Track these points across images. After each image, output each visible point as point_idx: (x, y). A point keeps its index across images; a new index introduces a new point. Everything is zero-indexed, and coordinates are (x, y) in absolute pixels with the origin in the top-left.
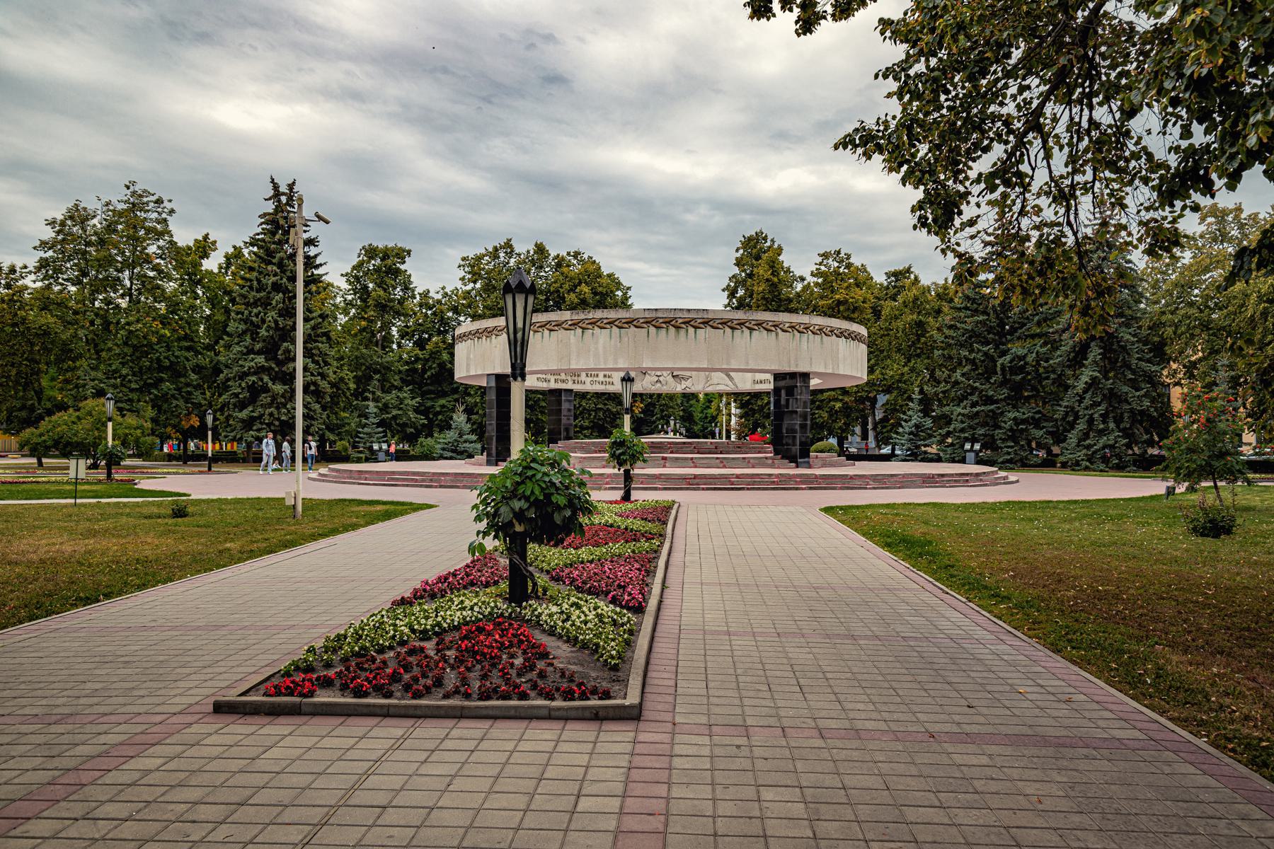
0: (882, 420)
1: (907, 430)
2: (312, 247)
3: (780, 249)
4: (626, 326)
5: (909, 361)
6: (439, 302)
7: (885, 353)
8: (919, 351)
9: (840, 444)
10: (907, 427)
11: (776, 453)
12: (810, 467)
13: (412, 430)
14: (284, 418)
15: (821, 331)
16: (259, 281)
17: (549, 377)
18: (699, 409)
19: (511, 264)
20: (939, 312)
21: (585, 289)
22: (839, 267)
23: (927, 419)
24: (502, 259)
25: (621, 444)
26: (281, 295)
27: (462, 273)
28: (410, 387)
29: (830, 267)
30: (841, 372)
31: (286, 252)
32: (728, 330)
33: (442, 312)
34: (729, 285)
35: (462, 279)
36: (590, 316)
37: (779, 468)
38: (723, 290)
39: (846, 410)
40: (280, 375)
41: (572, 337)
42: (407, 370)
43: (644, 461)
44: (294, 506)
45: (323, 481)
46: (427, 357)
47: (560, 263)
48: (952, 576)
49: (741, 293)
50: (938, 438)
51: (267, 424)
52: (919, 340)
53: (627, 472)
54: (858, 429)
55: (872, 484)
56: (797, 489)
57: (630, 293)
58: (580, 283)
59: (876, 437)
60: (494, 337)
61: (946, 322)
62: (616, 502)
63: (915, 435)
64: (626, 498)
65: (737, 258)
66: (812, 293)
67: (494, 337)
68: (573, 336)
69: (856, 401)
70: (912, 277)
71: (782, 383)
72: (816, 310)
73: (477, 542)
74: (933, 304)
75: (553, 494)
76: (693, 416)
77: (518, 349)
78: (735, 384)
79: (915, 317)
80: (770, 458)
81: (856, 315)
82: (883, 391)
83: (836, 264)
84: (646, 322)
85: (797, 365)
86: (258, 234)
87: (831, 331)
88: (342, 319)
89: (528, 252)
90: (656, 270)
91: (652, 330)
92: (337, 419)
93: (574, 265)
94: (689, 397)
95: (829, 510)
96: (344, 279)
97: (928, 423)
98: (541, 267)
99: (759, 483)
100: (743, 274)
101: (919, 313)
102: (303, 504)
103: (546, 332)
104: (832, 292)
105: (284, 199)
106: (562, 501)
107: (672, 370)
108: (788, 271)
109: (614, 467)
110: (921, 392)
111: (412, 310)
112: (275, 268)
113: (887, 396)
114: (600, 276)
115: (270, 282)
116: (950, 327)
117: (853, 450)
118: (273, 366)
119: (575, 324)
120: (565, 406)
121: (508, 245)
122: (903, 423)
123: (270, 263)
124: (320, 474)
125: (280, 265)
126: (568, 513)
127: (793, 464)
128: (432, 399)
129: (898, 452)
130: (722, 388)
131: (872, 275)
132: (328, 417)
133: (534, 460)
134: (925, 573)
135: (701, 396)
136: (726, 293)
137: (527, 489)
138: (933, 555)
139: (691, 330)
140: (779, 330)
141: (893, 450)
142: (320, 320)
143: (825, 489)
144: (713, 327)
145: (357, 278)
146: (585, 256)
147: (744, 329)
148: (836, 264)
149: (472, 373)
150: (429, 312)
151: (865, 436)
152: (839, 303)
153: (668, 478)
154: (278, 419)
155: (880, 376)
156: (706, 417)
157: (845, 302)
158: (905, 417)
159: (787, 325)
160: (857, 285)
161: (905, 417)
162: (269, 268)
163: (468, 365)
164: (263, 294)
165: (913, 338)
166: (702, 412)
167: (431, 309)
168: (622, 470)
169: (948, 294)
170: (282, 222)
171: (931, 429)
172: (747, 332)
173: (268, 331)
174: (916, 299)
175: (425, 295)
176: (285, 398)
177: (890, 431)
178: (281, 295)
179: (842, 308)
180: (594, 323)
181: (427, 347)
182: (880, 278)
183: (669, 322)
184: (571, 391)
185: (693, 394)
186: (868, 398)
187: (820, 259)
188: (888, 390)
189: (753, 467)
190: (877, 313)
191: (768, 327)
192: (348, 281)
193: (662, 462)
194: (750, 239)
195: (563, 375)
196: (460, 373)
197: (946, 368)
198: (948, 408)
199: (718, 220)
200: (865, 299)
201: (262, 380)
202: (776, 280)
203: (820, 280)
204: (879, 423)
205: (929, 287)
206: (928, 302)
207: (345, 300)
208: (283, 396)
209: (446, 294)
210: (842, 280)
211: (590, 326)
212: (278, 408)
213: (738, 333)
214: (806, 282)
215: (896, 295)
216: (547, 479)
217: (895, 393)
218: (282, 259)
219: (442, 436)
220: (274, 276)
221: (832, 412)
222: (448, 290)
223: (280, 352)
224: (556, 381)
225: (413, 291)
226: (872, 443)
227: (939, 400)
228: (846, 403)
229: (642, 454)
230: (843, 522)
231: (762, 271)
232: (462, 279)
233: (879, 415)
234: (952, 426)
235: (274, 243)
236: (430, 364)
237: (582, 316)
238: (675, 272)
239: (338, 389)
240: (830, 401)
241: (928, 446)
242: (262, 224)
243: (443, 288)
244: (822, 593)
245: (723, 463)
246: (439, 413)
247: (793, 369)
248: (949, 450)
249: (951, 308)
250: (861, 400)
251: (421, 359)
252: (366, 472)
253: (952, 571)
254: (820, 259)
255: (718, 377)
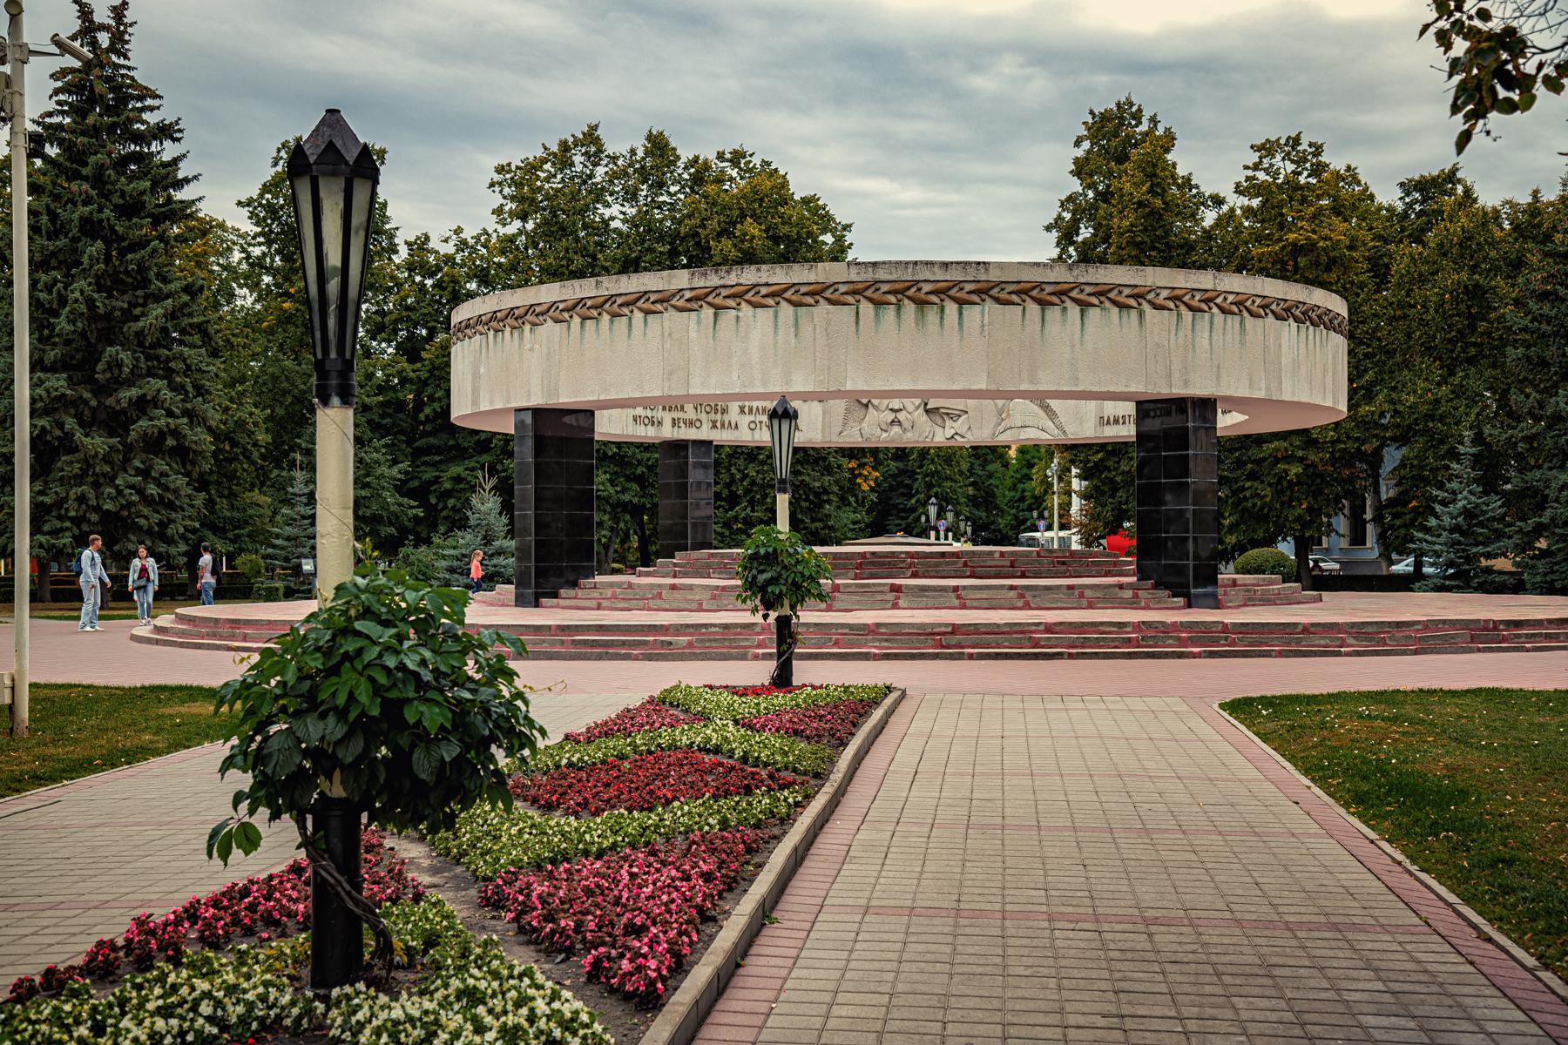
0: (1392, 502)
1: (1447, 520)
2: (167, 144)
3: (1170, 138)
4: (810, 300)
5: (1452, 373)
6: (449, 259)
7: (1398, 358)
8: (1473, 351)
9: (1302, 548)
10: (1446, 516)
11: (1142, 573)
12: (1217, 605)
13: (392, 530)
14: (109, 506)
15: (1240, 306)
16: (53, 216)
17: (659, 414)
18: (1008, 482)
19: (598, 179)
20: (1518, 264)
21: (752, 229)
22: (1297, 173)
23: (1494, 497)
24: (579, 168)
25: (770, 558)
26: (99, 244)
27: (497, 200)
28: (387, 440)
29: (1277, 173)
30: (1287, 397)
31: (109, 154)
32: (1033, 308)
33: (455, 281)
34: (1059, 218)
35: (498, 211)
36: (732, 279)
37: (1147, 608)
38: (1048, 228)
39: (1314, 481)
40: (103, 416)
41: (693, 325)
42: (381, 404)
43: (821, 597)
44: (11, 708)
45: (157, 642)
46: (424, 375)
47: (700, 174)
48: (1507, 890)
49: (1085, 233)
50: (1517, 539)
51: (72, 519)
52: (1473, 328)
53: (783, 623)
54: (1341, 523)
55: (1353, 644)
56: (1181, 656)
57: (849, 238)
58: (743, 216)
59: (1382, 537)
60: (527, 327)
61: (1535, 286)
62: (756, 691)
63: (1463, 533)
64: (783, 679)
65: (1076, 161)
66: (1239, 230)
67: (527, 327)
68: (693, 326)
69: (1333, 459)
70: (1460, 189)
71: (1154, 425)
72: (1244, 266)
73: (233, 825)
74: (1505, 247)
75: (408, 701)
76: (994, 496)
77: (332, 322)
78: (1060, 427)
79: (1464, 276)
80: (1130, 586)
81: (1333, 276)
82: (1394, 439)
83: (1290, 167)
84: (854, 293)
85: (1186, 383)
86: (50, 114)
87: (1264, 307)
88: (246, 298)
89: (633, 152)
90: (912, 193)
91: (866, 308)
92: (232, 507)
93: (731, 179)
94: (987, 454)
95: (1241, 708)
96: (245, 212)
97: (1495, 505)
98: (661, 185)
99: (1097, 643)
100: (1091, 194)
101: (1474, 269)
102: (33, 700)
103: (638, 315)
104: (1281, 227)
105: (104, 39)
106: (433, 717)
107: (925, 395)
108: (1187, 182)
109: (755, 610)
110: (1478, 439)
111: (393, 278)
112: (86, 186)
113: (1404, 450)
114: (785, 200)
115: (76, 216)
116: (1544, 296)
117: (1330, 566)
118: (87, 395)
119: (699, 299)
120: (695, 476)
121: (591, 138)
122: (1438, 508)
123: (77, 176)
124: (158, 630)
125: (98, 180)
126: (449, 752)
127: (1180, 601)
128: (434, 465)
129: (1427, 570)
130: (1031, 435)
131: (1372, 189)
132: (210, 503)
133: (367, 613)
134: (1438, 879)
135: (1012, 453)
136: (1055, 234)
137: (337, 690)
138: (1465, 828)
139: (951, 308)
140: (1146, 306)
141: (1418, 565)
142: (186, 298)
143: (1245, 655)
144: (998, 301)
145: (272, 210)
146: (756, 161)
147: (1069, 303)
148: (1290, 167)
149: (485, 406)
150: (429, 282)
151: (1358, 538)
152: (1297, 249)
153: (894, 632)
154: (97, 509)
155: (1386, 406)
156: (1022, 499)
157: (1312, 246)
158: (1441, 494)
159: (1165, 293)
160: (1337, 210)
161: (1441, 494)
162: (74, 186)
163: (476, 390)
164: (62, 242)
165: (1460, 323)
166: (1014, 488)
167: (431, 275)
168: (773, 615)
169: (1540, 225)
170: (101, 87)
171: (1502, 519)
172: (1074, 310)
173: (74, 322)
174: (1468, 237)
175: (420, 246)
176: (110, 463)
177: (1412, 524)
178: (99, 244)
179: (1302, 261)
180: (739, 296)
181: (424, 355)
182: (1388, 195)
183: (902, 292)
184: (706, 444)
185: (993, 449)
186: (1360, 455)
187: (1255, 157)
188: (1403, 439)
189: (1091, 606)
190: (1379, 269)
191: (1121, 299)
192: (252, 215)
193: (891, 596)
194: (1105, 117)
195: (689, 407)
196: (461, 410)
197: (1535, 387)
198: (1538, 474)
199: (1039, 88)
200: (1353, 239)
201: (61, 425)
202: (1158, 202)
203: (1256, 202)
204: (1387, 506)
205: (1495, 210)
206: (1493, 244)
207: (248, 257)
208: (107, 459)
209: (464, 242)
210: (1304, 200)
211: (731, 303)
212: (96, 485)
213: (1053, 313)
214: (1225, 208)
215: (1423, 230)
216: (391, 662)
217: (1420, 442)
218: (101, 167)
219: (450, 542)
220: (86, 203)
221: (1282, 486)
222: (468, 234)
223: (100, 367)
224: (675, 423)
225: (391, 237)
226: (1372, 549)
227: (1519, 457)
228: (1313, 465)
229: (813, 579)
230: (1265, 738)
231: (1130, 184)
232: (498, 211)
233: (1387, 492)
234: (1548, 513)
235: (83, 133)
236: (429, 390)
237: (714, 280)
238: (953, 197)
239: (234, 444)
240: (1277, 461)
241: (1495, 556)
242: (57, 92)
243: (458, 231)
244: (1164, 938)
245: (1025, 599)
246: (448, 494)
247: (1178, 390)
248: (1541, 565)
249: (1546, 255)
250: (1347, 459)
251: (410, 381)
252: (248, 623)
253: (1510, 876)
254: (1255, 157)
255: (1022, 409)
